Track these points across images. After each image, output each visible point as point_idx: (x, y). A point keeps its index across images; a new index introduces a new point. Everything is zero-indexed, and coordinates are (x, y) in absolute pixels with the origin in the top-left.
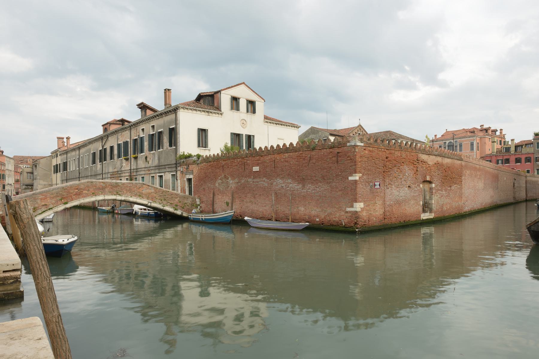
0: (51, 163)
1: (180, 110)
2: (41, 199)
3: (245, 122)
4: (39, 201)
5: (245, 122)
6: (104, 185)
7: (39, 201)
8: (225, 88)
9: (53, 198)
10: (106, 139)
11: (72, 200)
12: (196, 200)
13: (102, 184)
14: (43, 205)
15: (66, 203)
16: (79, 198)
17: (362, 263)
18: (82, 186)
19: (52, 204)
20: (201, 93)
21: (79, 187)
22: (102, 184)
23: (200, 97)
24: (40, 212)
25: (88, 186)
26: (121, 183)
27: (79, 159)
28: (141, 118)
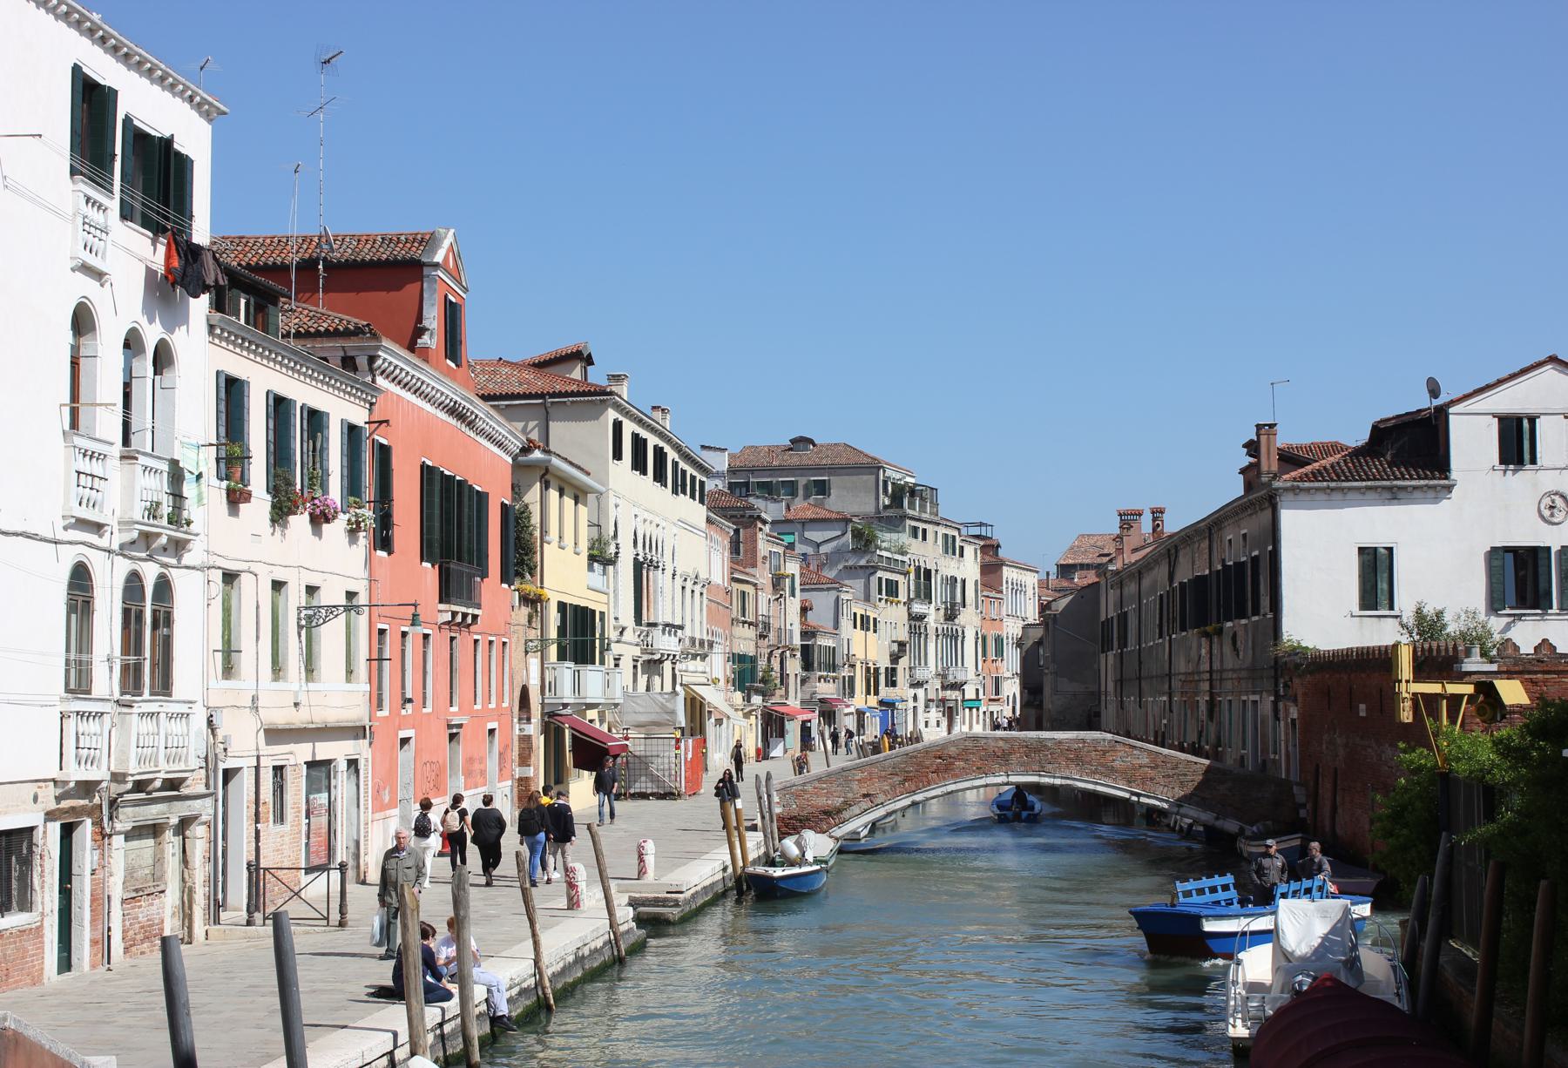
0: (397, 735)
1: (1283, 498)
2: (859, 780)
3: (1547, 513)
4: (855, 786)
5: (1547, 513)
6: (1006, 746)
7: (855, 786)
8: (1517, 370)
9: (885, 778)
10: (279, 873)
11: (929, 784)
12: (1292, 788)
13: (1001, 743)
14: (865, 796)
15: (914, 792)
16: (944, 779)
17: (1166, 801)
18: (952, 749)
19: (885, 792)
20: (1382, 421)
21: (946, 752)
22: (1001, 743)
23: (1381, 433)
24: (858, 812)
25: (965, 750)
26: (1050, 739)
27: (257, 768)
28: (1242, 493)
